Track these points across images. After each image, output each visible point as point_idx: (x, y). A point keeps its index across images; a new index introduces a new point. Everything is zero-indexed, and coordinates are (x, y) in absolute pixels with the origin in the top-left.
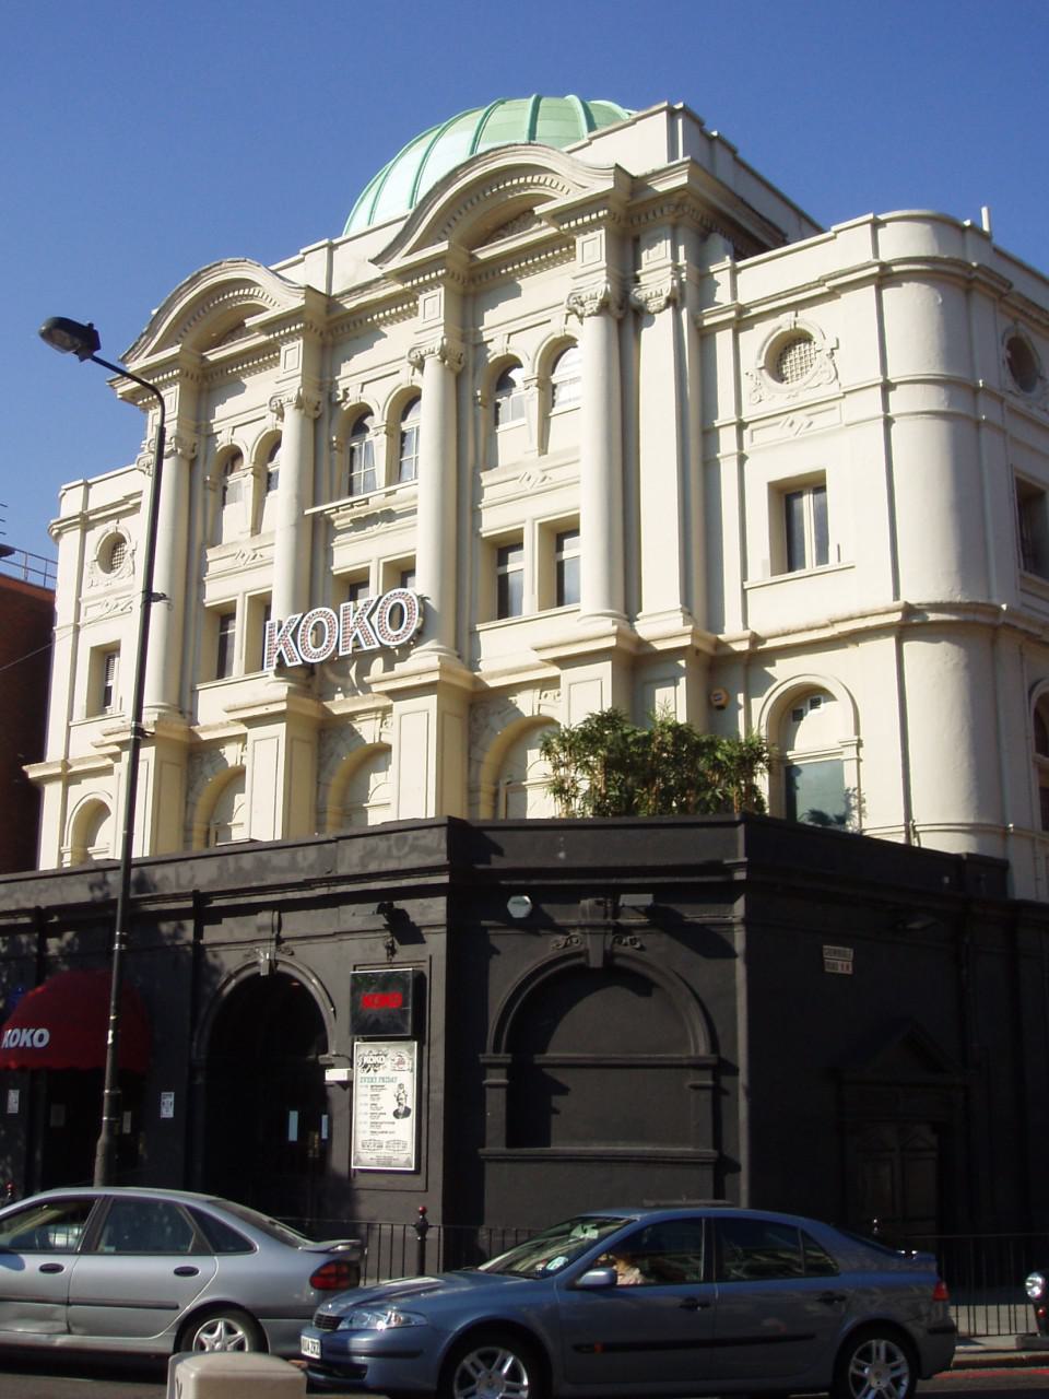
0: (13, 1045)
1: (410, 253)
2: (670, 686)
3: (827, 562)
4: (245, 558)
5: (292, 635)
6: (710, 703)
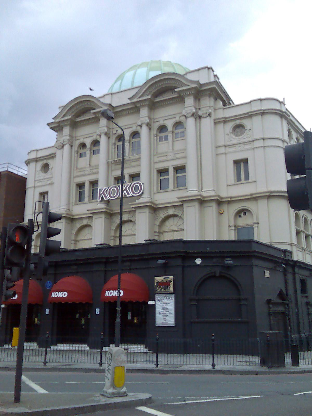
0: (56, 296)
1: (61, 118)
2: (42, 220)
3: (249, 180)
4: (239, 139)
5: (128, 188)
6: (219, 213)
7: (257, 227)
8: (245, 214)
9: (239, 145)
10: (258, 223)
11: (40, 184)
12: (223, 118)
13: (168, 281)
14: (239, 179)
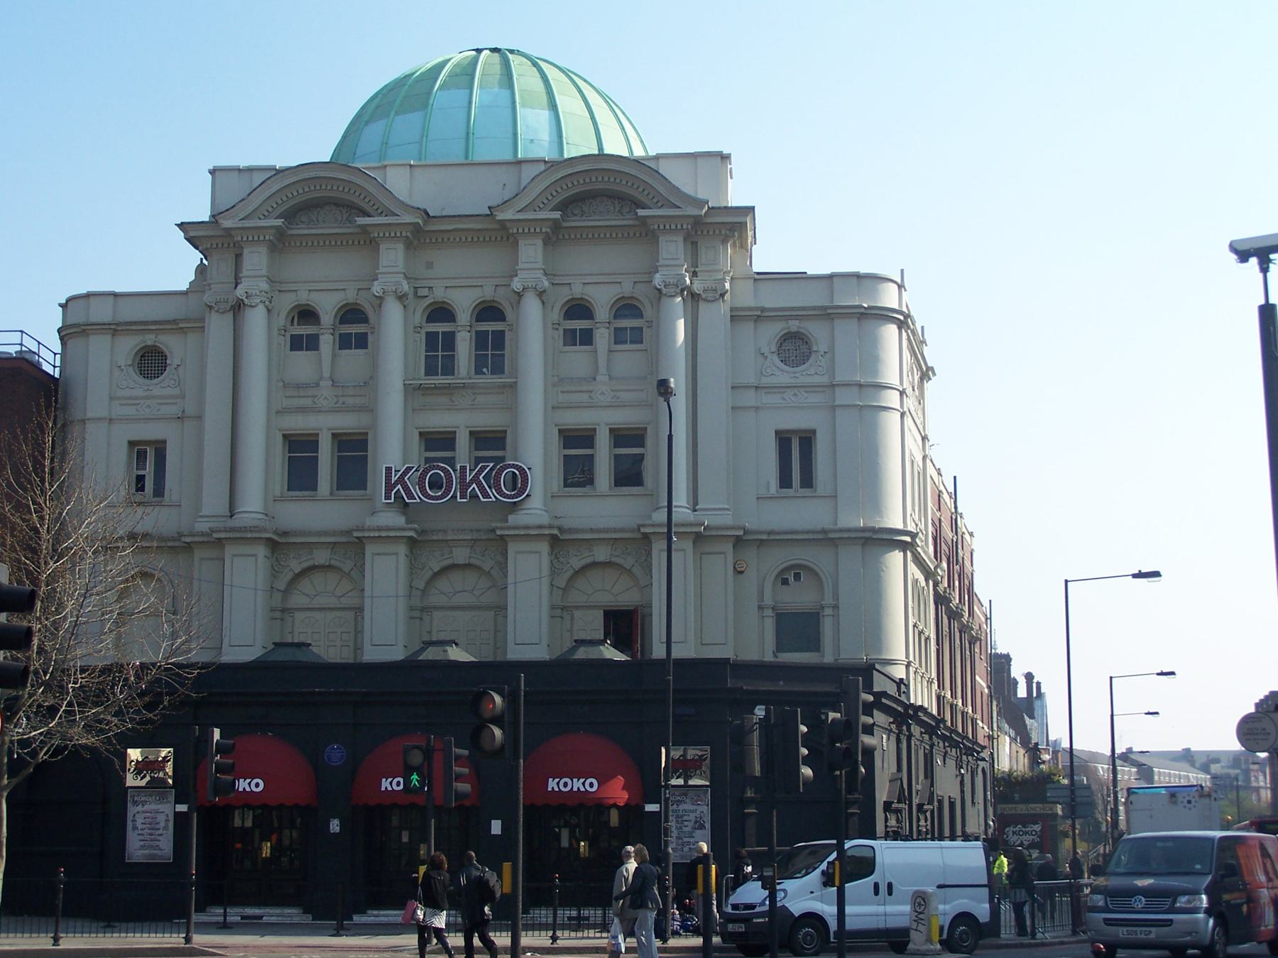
7: (833, 616)
8: (797, 576)
9: (796, 391)
10: (836, 607)
11: (130, 411)
12: (757, 309)
13: (697, 757)
14: (785, 481)
